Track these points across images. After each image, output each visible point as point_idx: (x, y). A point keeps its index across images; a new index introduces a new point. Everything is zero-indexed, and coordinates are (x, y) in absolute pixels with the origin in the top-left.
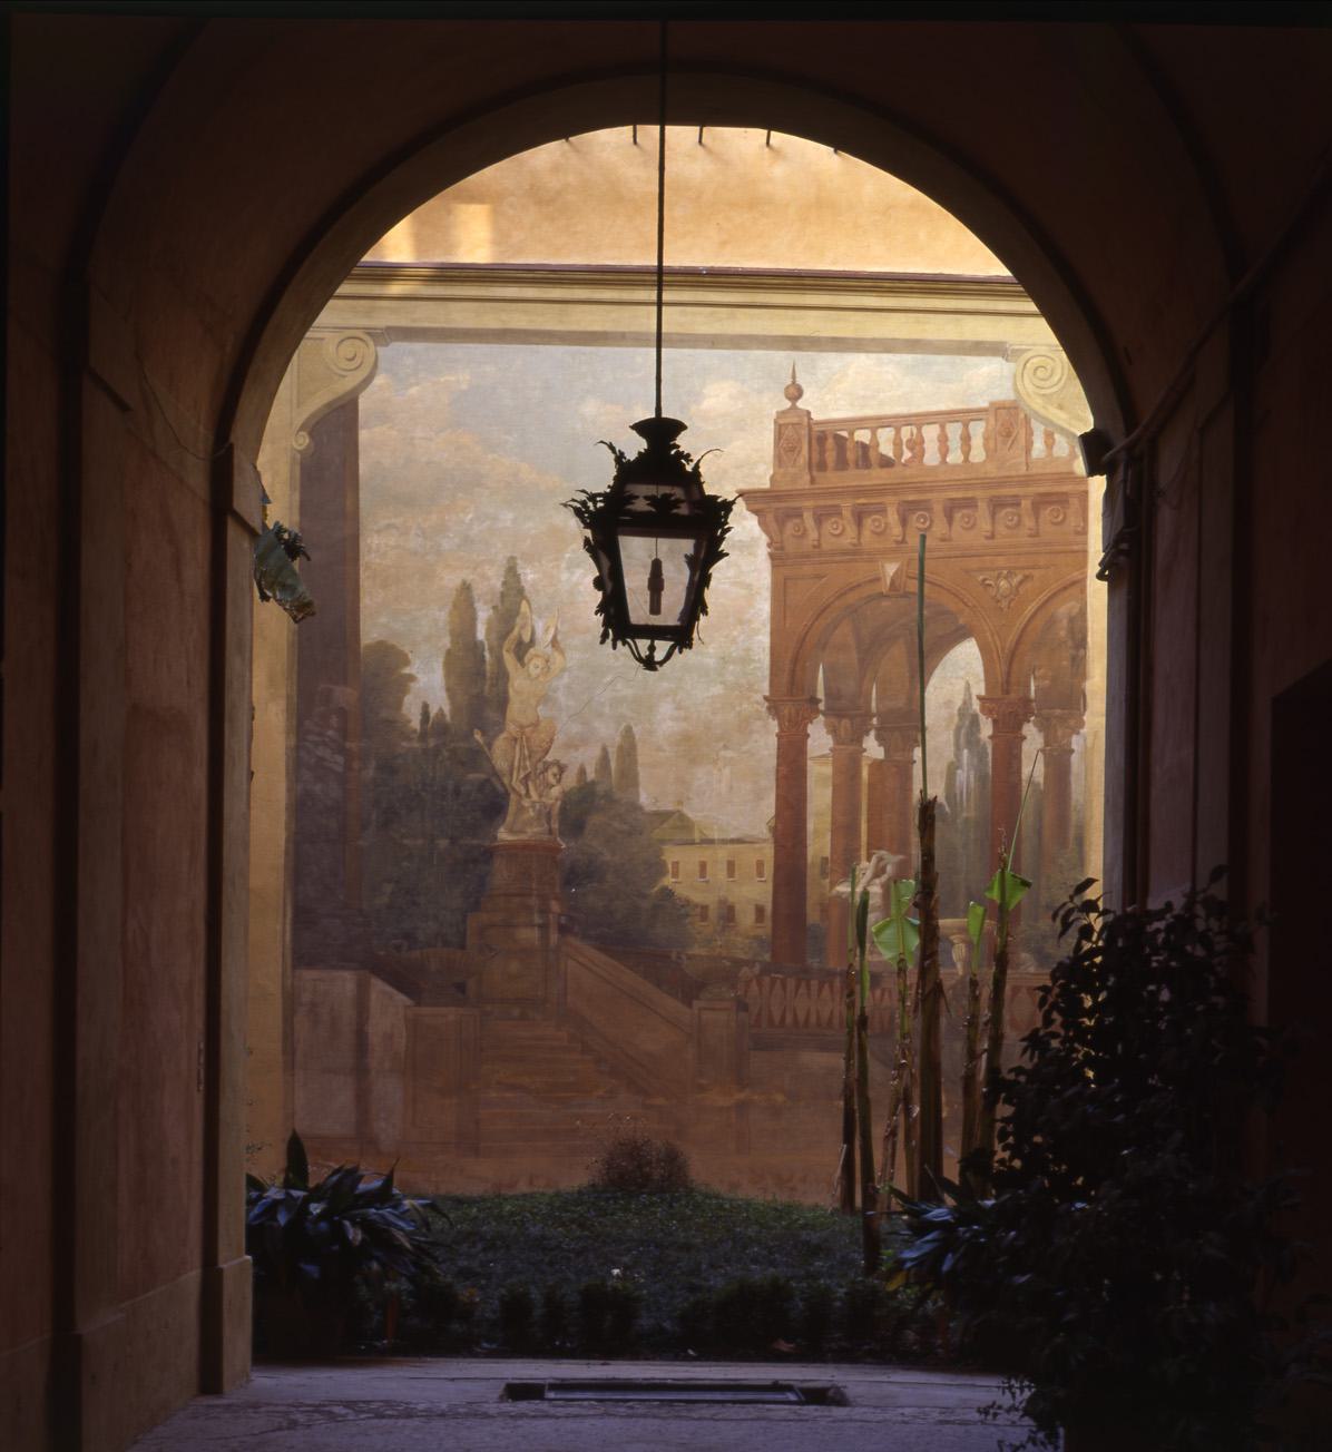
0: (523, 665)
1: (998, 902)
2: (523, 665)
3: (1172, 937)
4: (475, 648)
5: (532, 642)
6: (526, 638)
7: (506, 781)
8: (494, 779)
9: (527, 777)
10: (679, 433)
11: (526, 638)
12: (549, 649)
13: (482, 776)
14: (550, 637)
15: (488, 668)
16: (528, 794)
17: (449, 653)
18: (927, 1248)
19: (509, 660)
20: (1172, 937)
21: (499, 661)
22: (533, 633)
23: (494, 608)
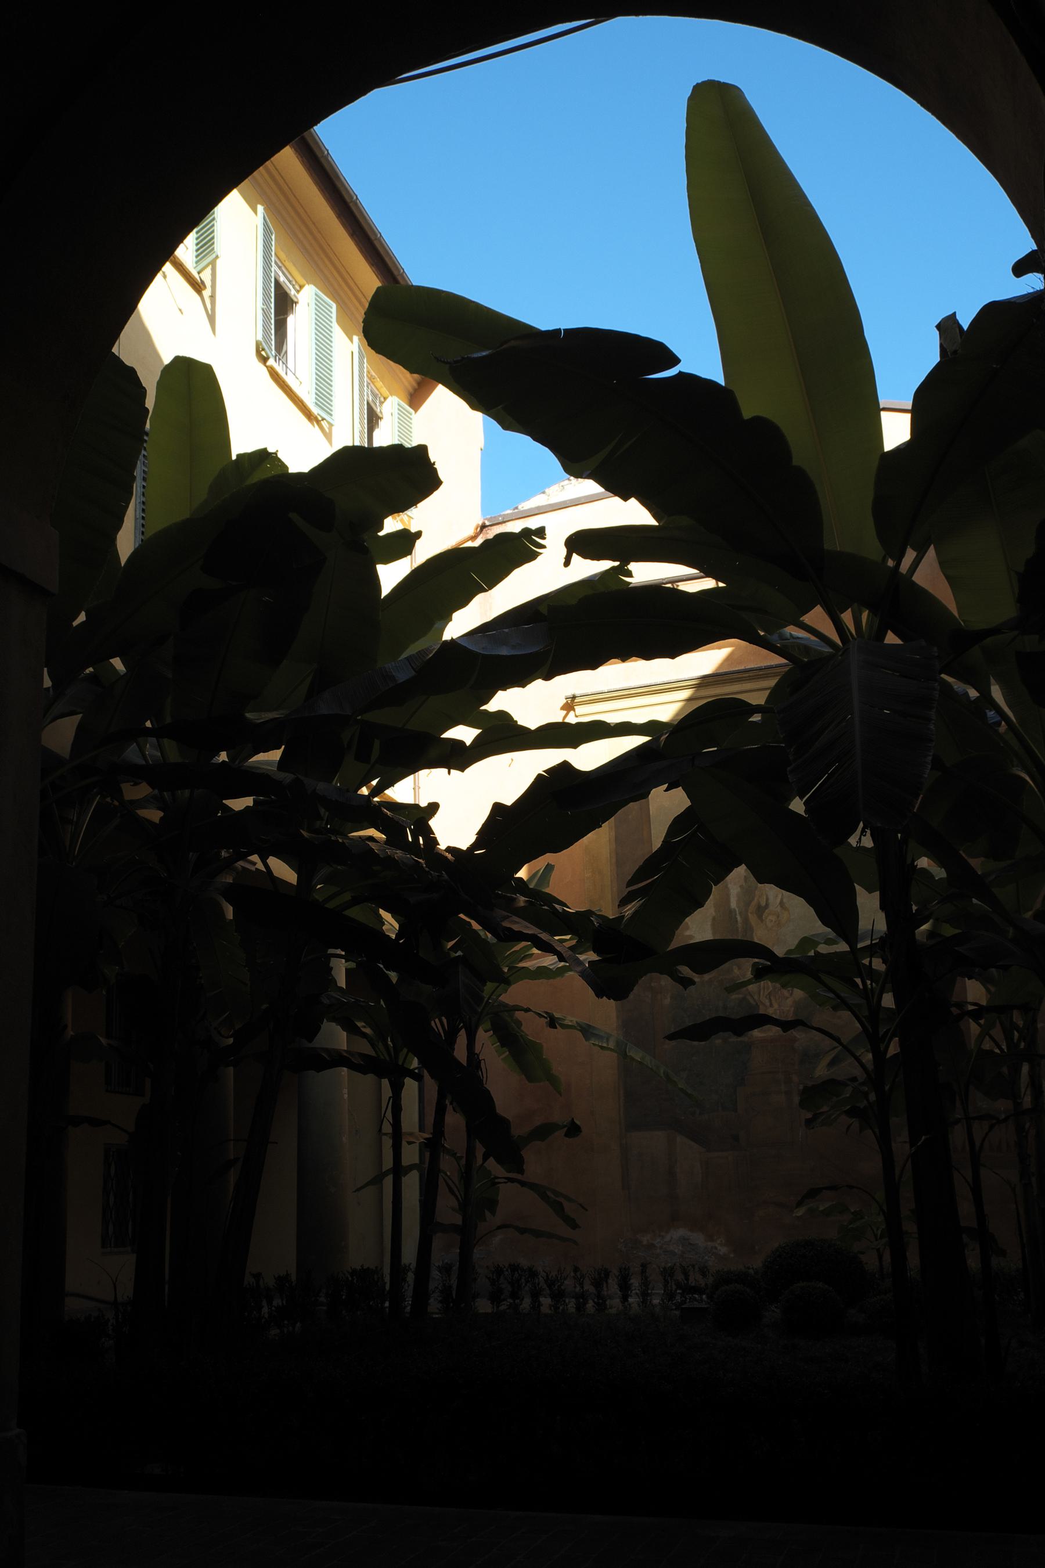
0: (762, 921)
1: (983, 859)
2: (762, 921)
3: (756, 718)
4: (731, 912)
5: (767, 906)
6: (763, 904)
7: (756, 997)
8: (749, 997)
9: (769, 994)
10: (115, 539)
11: (763, 904)
12: (779, 909)
13: (741, 996)
14: (779, 900)
15: (740, 925)
16: (771, 1005)
17: (714, 919)
18: (1029, 1092)
19: (753, 919)
20: (756, 718)
21: (746, 920)
22: (767, 899)
23: (741, 887)
